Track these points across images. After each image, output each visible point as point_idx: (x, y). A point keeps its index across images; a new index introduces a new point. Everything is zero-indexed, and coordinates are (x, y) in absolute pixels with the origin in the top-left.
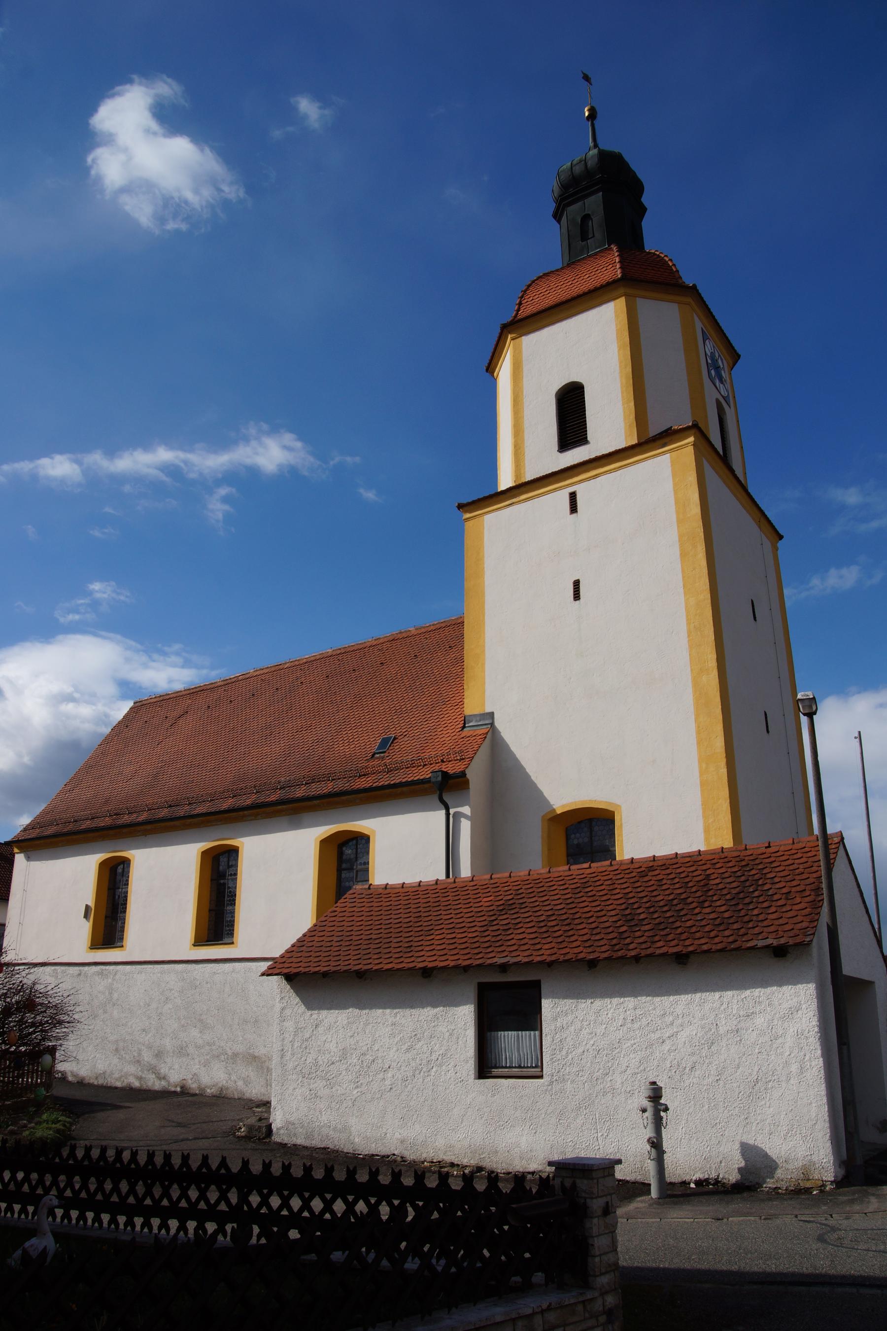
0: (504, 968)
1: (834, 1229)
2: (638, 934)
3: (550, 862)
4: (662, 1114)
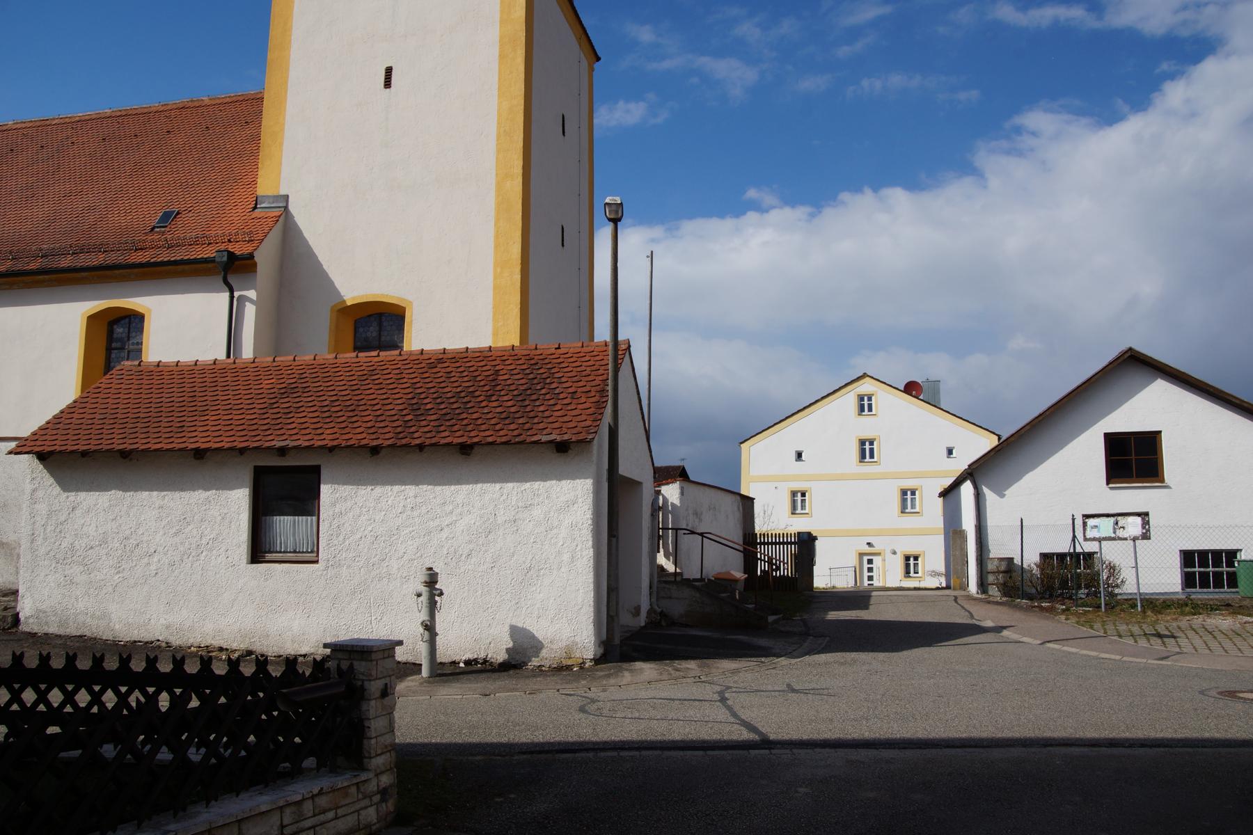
0: (282, 451)
1: (593, 701)
2: (423, 423)
3: (337, 348)
4: (437, 598)
